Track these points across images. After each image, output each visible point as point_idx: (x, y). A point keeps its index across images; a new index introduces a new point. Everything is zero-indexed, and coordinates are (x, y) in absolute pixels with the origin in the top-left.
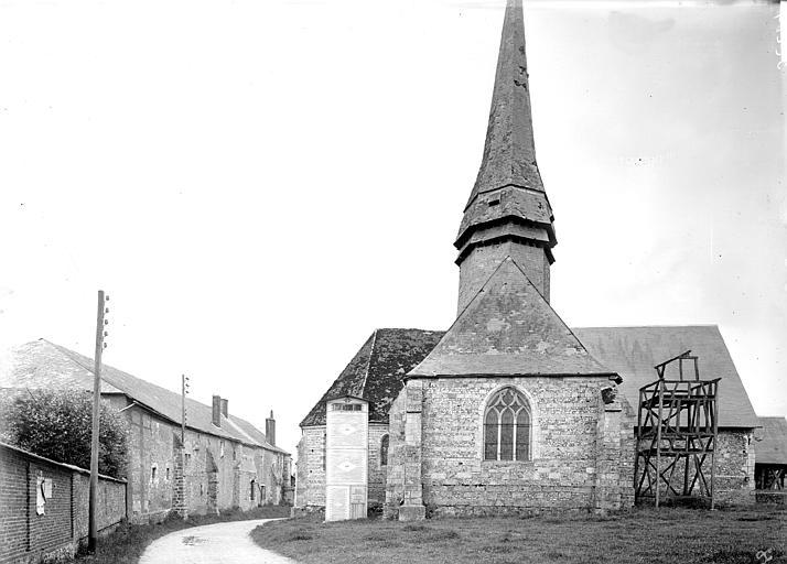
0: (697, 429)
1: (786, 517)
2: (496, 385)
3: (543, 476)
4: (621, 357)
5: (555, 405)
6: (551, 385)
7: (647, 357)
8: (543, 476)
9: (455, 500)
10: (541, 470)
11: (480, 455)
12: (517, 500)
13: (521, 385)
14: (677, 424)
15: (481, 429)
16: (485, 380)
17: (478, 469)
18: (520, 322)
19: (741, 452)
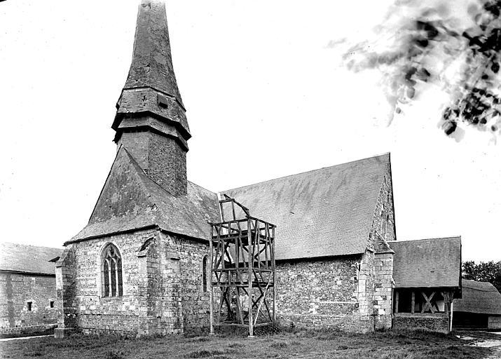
0: (237, 266)
1: (497, 343)
2: (103, 243)
3: (127, 308)
4: (289, 200)
5: (131, 254)
6: (128, 239)
7: (308, 197)
8: (127, 308)
9: (90, 325)
10: (126, 304)
11: (99, 294)
12: (115, 325)
13: (115, 241)
14: (272, 256)
15: (99, 275)
16: (98, 240)
17: (98, 303)
18: (126, 193)
19: (352, 279)
